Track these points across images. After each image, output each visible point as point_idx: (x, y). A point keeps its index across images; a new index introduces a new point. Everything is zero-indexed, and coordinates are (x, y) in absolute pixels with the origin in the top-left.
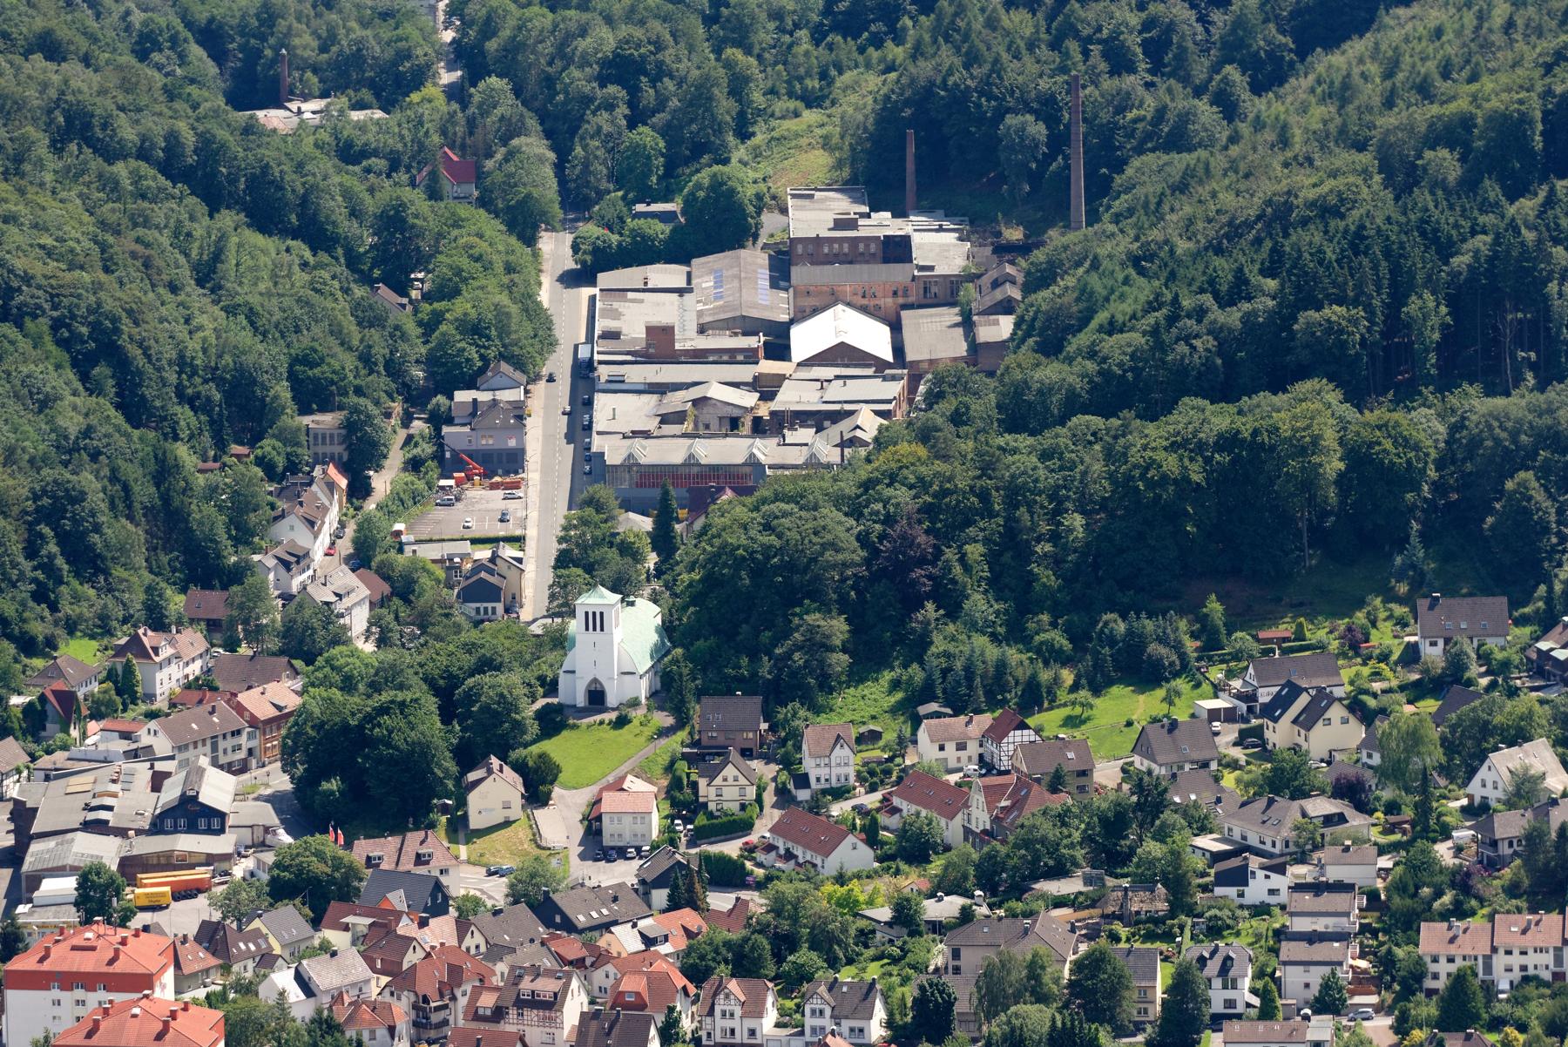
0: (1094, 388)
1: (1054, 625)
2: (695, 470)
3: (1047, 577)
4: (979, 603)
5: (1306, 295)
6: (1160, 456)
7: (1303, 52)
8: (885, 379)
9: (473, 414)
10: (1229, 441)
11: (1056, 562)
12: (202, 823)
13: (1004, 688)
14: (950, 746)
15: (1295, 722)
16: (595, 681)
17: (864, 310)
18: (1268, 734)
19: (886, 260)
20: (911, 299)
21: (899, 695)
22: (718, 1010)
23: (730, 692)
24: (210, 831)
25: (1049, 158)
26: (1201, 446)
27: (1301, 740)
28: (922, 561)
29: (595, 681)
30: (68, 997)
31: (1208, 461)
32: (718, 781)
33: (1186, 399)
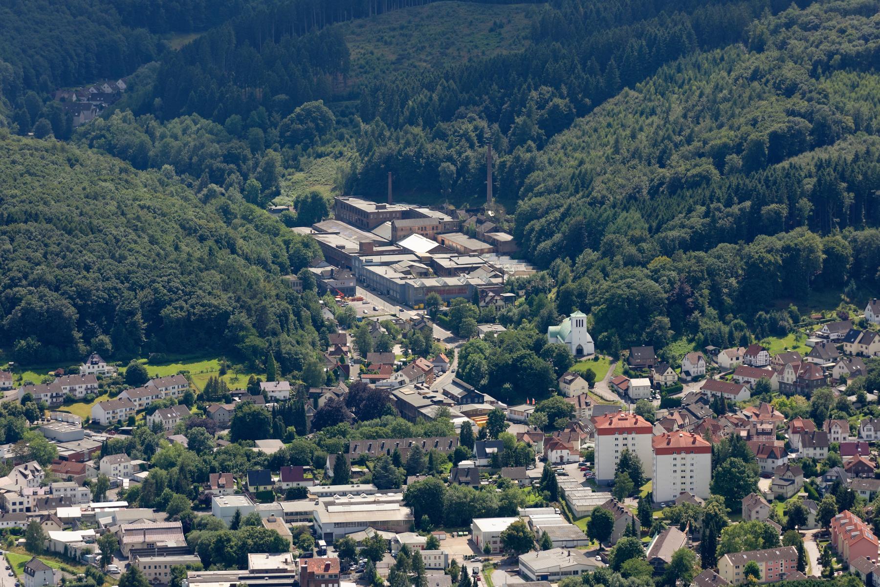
0: (692, 238)
1: (735, 318)
2: (447, 288)
3: (728, 301)
4: (711, 311)
5: (761, 201)
6: (764, 255)
7: (549, 136)
8: (470, 256)
9: (332, 274)
10: (787, 249)
11: (729, 295)
12: (476, 400)
13: (734, 340)
14: (734, 359)
15: (860, 342)
16: (580, 345)
17: (422, 235)
18: (845, 348)
19: (403, 218)
20: (439, 231)
21: (694, 344)
22: (832, 431)
23: (640, 345)
24: (479, 403)
25: (458, 178)
26: (777, 251)
27: (864, 349)
28: (689, 297)
29: (580, 345)
30: (621, 437)
31: (781, 256)
32: (665, 374)
33: (416, 286)
